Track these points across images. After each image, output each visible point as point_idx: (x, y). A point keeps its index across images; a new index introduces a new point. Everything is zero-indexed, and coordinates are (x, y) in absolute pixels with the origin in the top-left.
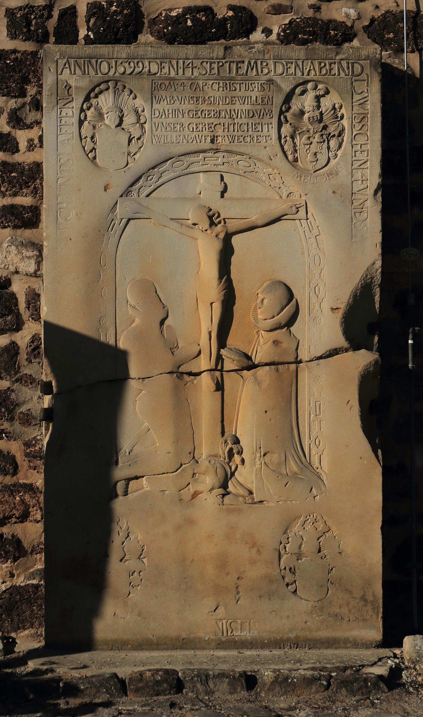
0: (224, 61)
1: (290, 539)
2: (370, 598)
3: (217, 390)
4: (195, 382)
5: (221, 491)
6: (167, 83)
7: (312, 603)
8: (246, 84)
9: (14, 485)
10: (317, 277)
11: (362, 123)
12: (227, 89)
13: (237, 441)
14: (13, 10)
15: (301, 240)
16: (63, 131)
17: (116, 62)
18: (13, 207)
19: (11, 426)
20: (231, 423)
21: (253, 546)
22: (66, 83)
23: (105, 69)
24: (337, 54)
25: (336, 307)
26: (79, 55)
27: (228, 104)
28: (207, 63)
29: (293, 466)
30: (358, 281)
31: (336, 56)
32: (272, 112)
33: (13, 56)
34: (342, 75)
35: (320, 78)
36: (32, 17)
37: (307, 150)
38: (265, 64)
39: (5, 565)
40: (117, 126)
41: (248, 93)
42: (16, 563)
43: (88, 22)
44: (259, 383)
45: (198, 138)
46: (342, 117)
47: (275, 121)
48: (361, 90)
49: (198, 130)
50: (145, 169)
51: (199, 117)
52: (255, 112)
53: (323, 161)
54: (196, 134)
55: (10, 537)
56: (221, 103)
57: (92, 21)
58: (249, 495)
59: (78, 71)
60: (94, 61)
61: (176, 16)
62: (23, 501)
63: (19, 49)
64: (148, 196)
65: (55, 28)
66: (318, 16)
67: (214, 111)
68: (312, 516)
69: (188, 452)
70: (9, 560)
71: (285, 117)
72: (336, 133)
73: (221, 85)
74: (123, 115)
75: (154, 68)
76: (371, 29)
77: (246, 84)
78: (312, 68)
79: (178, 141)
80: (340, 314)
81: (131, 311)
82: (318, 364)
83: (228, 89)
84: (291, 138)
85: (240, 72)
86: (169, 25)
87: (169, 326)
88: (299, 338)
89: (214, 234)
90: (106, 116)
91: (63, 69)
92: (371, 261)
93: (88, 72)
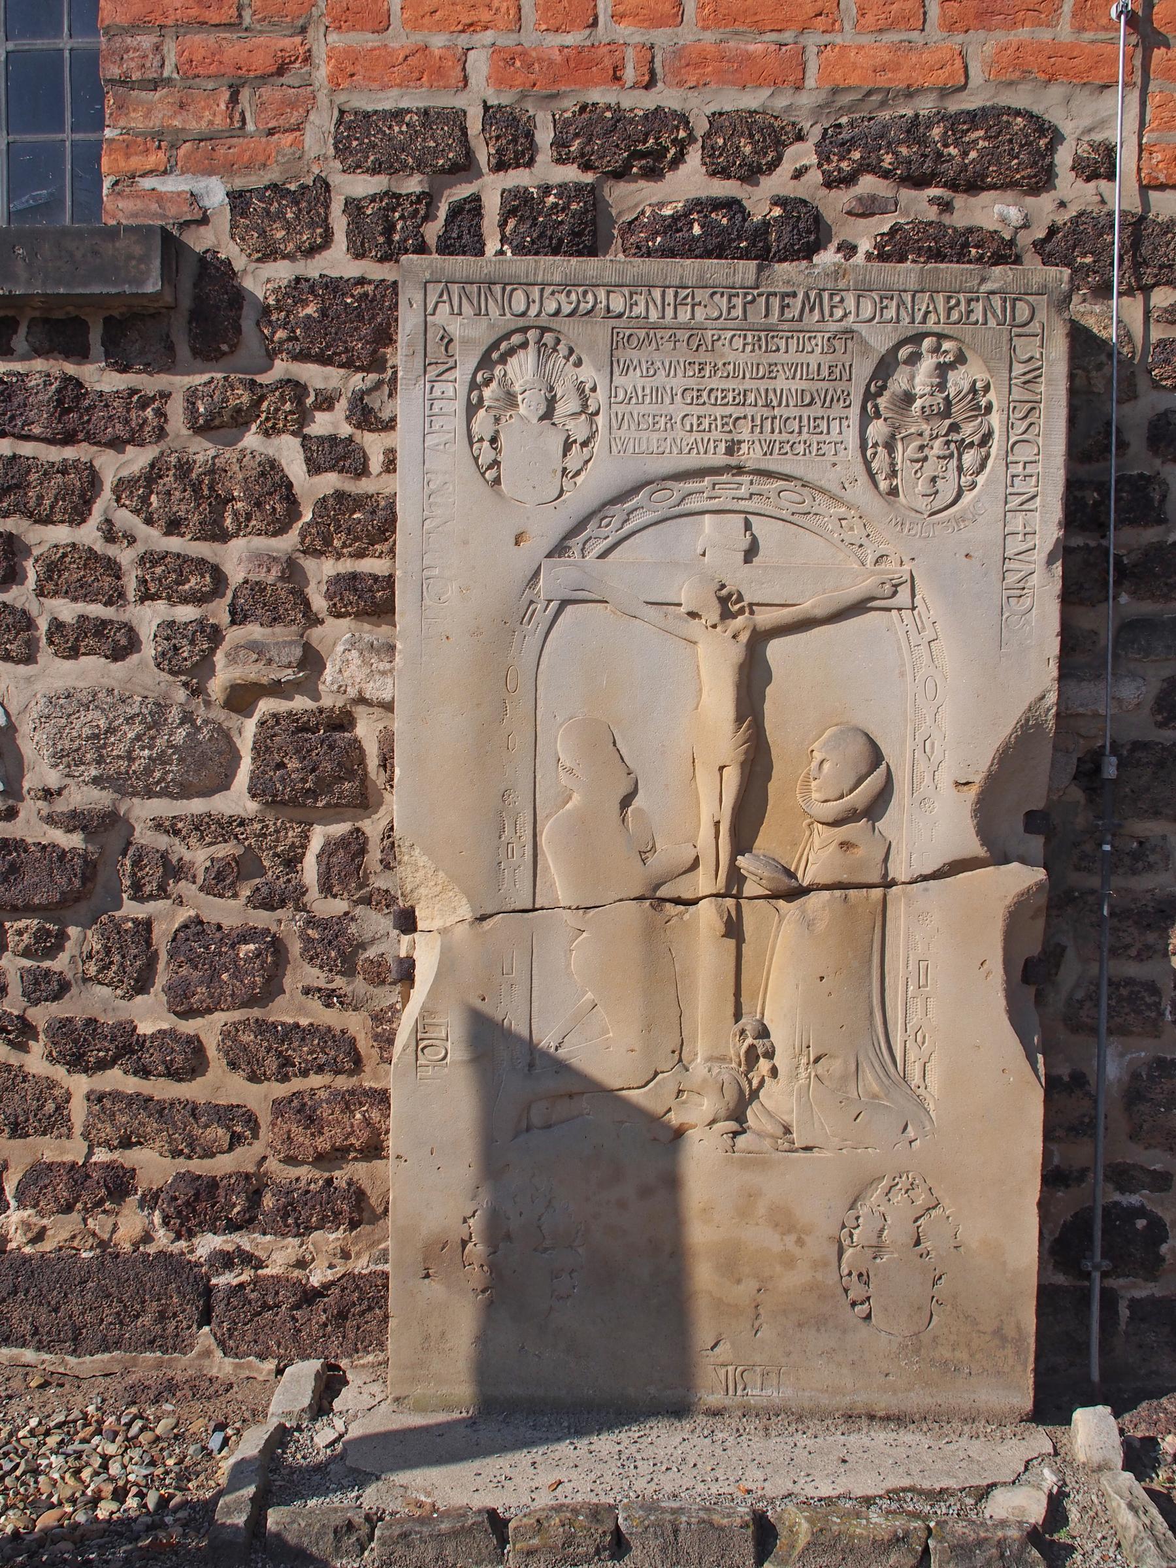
0: (755, 292)
1: (860, 1220)
2: (1010, 1332)
3: (727, 935)
4: (686, 917)
5: (732, 1125)
6: (642, 333)
7: (900, 1339)
8: (798, 338)
9: (352, 1092)
10: (929, 720)
11: (1028, 421)
12: (760, 347)
13: (763, 1033)
14: (360, 200)
15: (900, 648)
16: (436, 427)
17: (542, 291)
18: (354, 576)
19: (348, 983)
20: (754, 997)
21: (789, 1232)
22: (442, 332)
23: (519, 303)
24: (983, 280)
25: (964, 781)
26: (468, 277)
27: (763, 378)
28: (722, 295)
29: (870, 1080)
30: (1009, 730)
31: (980, 284)
32: (848, 395)
33: (358, 291)
34: (992, 323)
35: (947, 330)
36: (397, 215)
37: (916, 472)
38: (837, 299)
39: (333, 1236)
40: (541, 419)
41: (803, 358)
42: (354, 1233)
43: (503, 225)
44: (810, 925)
45: (700, 445)
46: (989, 408)
47: (854, 412)
48: (1028, 355)
49: (702, 428)
50: (595, 504)
51: (704, 403)
52: (815, 395)
53: (949, 494)
54: (699, 436)
55: (344, 1185)
56: (748, 376)
57: (512, 223)
58: (785, 1134)
59: (467, 309)
60: (498, 289)
61: (672, 216)
62: (367, 1121)
63: (369, 277)
64: (603, 555)
65: (439, 237)
66: (947, 219)
67: (734, 390)
68: (904, 1178)
69: (670, 1050)
70: (342, 1227)
71: (876, 407)
72: (976, 439)
73: (749, 339)
74: (555, 395)
75: (618, 303)
76: (1048, 248)
77: (798, 338)
78: (931, 308)
79: (661, 449)
80: (972, 793)
81: (564, 778)
82: (926, 890)
83: (764, 348)
84: (885, 447)
85: (788, 315)
86: (657, 233)
87: (639, 810)
88: (890, 838)
89: (729, 634)
90: (520, 398)
91: (437, 303)
92: (1037, 693)
93: (487, 309)
